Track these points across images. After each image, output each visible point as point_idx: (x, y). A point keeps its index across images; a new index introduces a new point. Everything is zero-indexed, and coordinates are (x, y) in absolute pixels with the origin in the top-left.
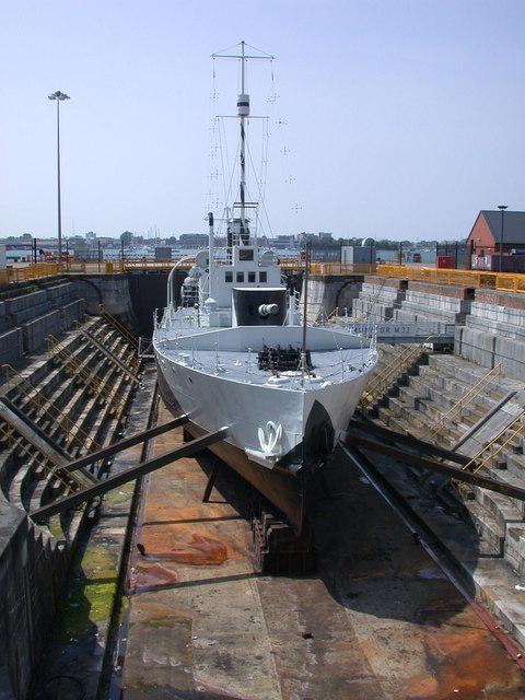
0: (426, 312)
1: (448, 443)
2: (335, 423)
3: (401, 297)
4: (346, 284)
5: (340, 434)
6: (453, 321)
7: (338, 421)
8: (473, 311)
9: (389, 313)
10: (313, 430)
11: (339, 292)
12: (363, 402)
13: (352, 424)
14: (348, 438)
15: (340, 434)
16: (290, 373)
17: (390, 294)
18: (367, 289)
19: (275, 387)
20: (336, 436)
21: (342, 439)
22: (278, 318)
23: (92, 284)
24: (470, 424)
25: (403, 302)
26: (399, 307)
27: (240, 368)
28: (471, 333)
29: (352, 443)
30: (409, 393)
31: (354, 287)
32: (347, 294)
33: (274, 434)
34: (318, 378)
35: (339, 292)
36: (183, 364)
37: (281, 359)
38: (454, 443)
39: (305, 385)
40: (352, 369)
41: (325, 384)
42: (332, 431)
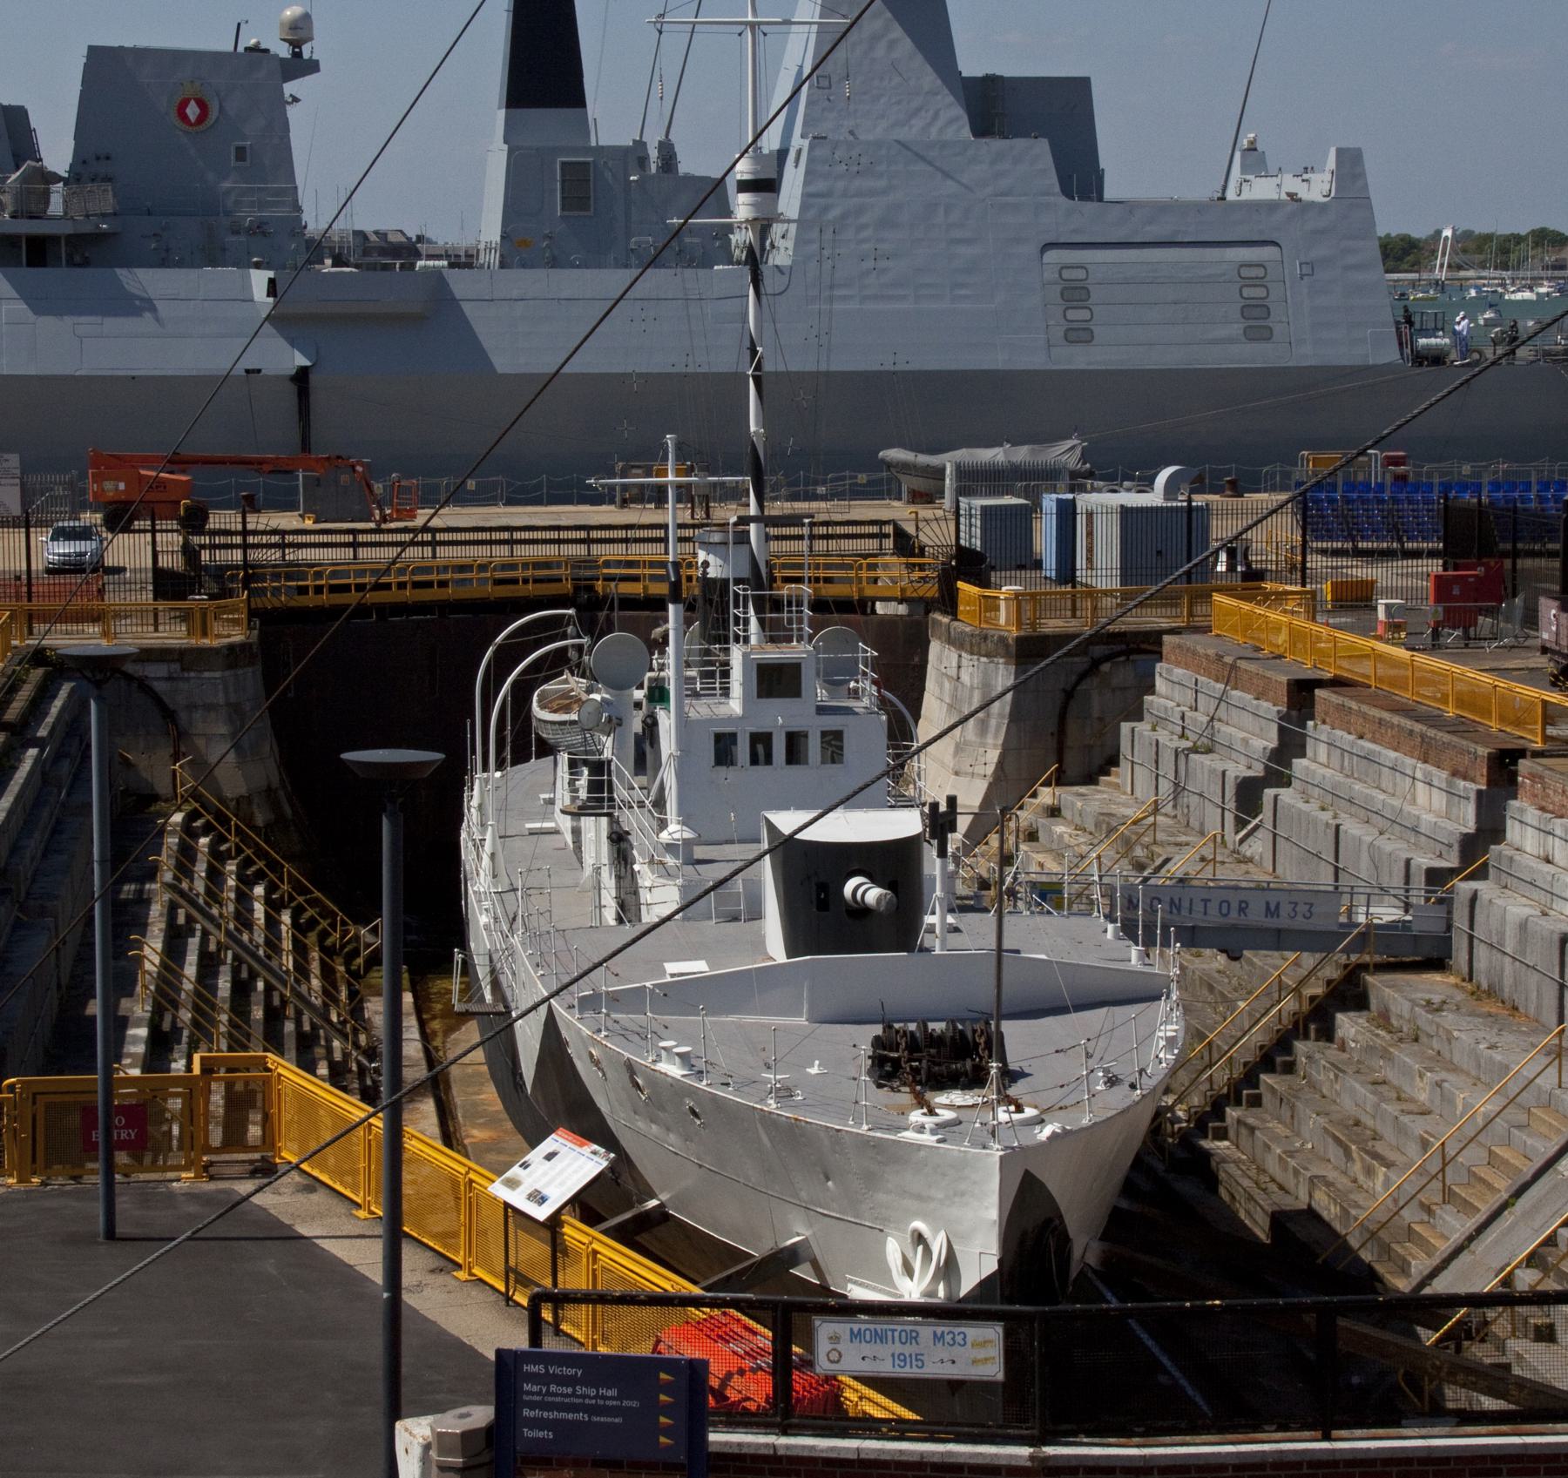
0: (1368, 813)
1: (1404, 1270)
2: (1073, 1223)
3: (1290, 746)
4: (1095, 664)
5: (1085, 1248)
6: (1451, 861)
7: (1081, 1209)
8: (1513, 831)
9: (1248, 796)
10: (1022, 1243)
11: (1069, 694)
12: (1160, 1116)
13: (1116, 1216)
14: (1106, 1260)
15: (1085, 1248)
16: (957, 1097)
17: (1251, 732)
18: (1172, 688)
19: (928, 1139)
20: (1077, 1253)
21: (1092, 1260)
22: (898, 927)
23: (143, 685)
24: (1467, 1207)
25: (1299, 764)
26: (1286, 782)
27: (816, 1066)
28: (1504, 907)
29: (1113, 1272)
30: (1509, 880)
31: (1122, 674)
32: (1096, 699)
33: (928, 1252)
34: (1030, 1112)
35: (1069, 694)
36: (674, 1070)
37: (938, 1056)
38: (1420, 1265)
39: (1001, 1133)
40: (1112, 1081)
41: (1048, 1131)
42: (1064, 1240)
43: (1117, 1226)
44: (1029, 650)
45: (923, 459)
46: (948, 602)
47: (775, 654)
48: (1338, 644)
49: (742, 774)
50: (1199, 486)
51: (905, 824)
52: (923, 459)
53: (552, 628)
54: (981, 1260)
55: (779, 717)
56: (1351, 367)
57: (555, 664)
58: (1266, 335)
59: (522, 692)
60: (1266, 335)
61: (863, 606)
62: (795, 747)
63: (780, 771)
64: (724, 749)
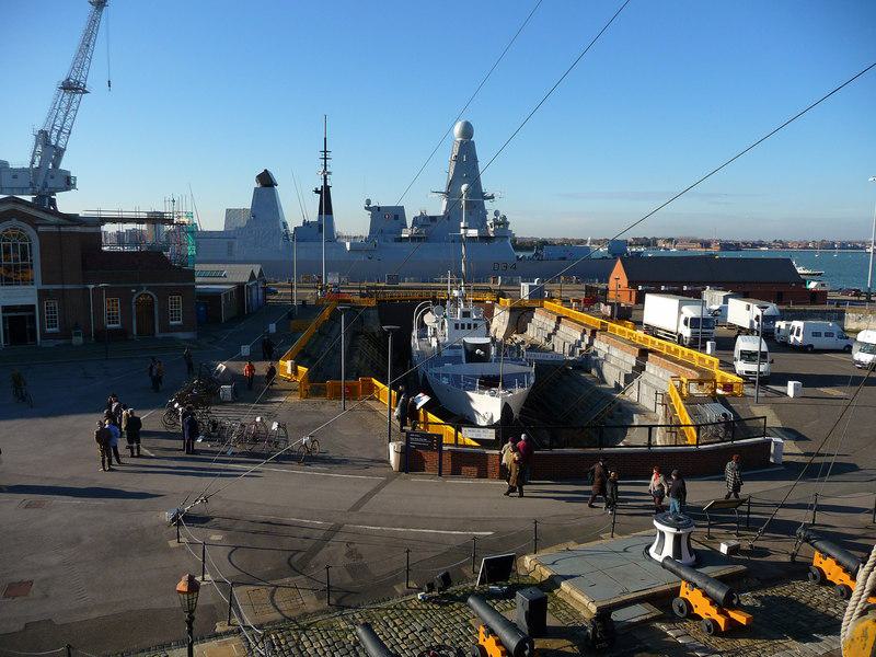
5: (516, 414)
15: (516, 414)
18: (538, 317)
43: (522, 412)
44: (512, 310)
45: (167, 335)
46: (498, 301)
47: (466, 310)
48: (565, 310)
49: (460, 331)
50: (543, 282)
51: (488, 340)
52: (167, 335)
53: (427, 304)
54: (497, 418)
55: (466, 321)
56: (22, 306)
57: (426, 312)
58: (231, 255)
59: (423, 315)
60: (231, 255)
61: (483, 301)
62: (469, 327)
63: (466, 331)
64: (457, 326)
